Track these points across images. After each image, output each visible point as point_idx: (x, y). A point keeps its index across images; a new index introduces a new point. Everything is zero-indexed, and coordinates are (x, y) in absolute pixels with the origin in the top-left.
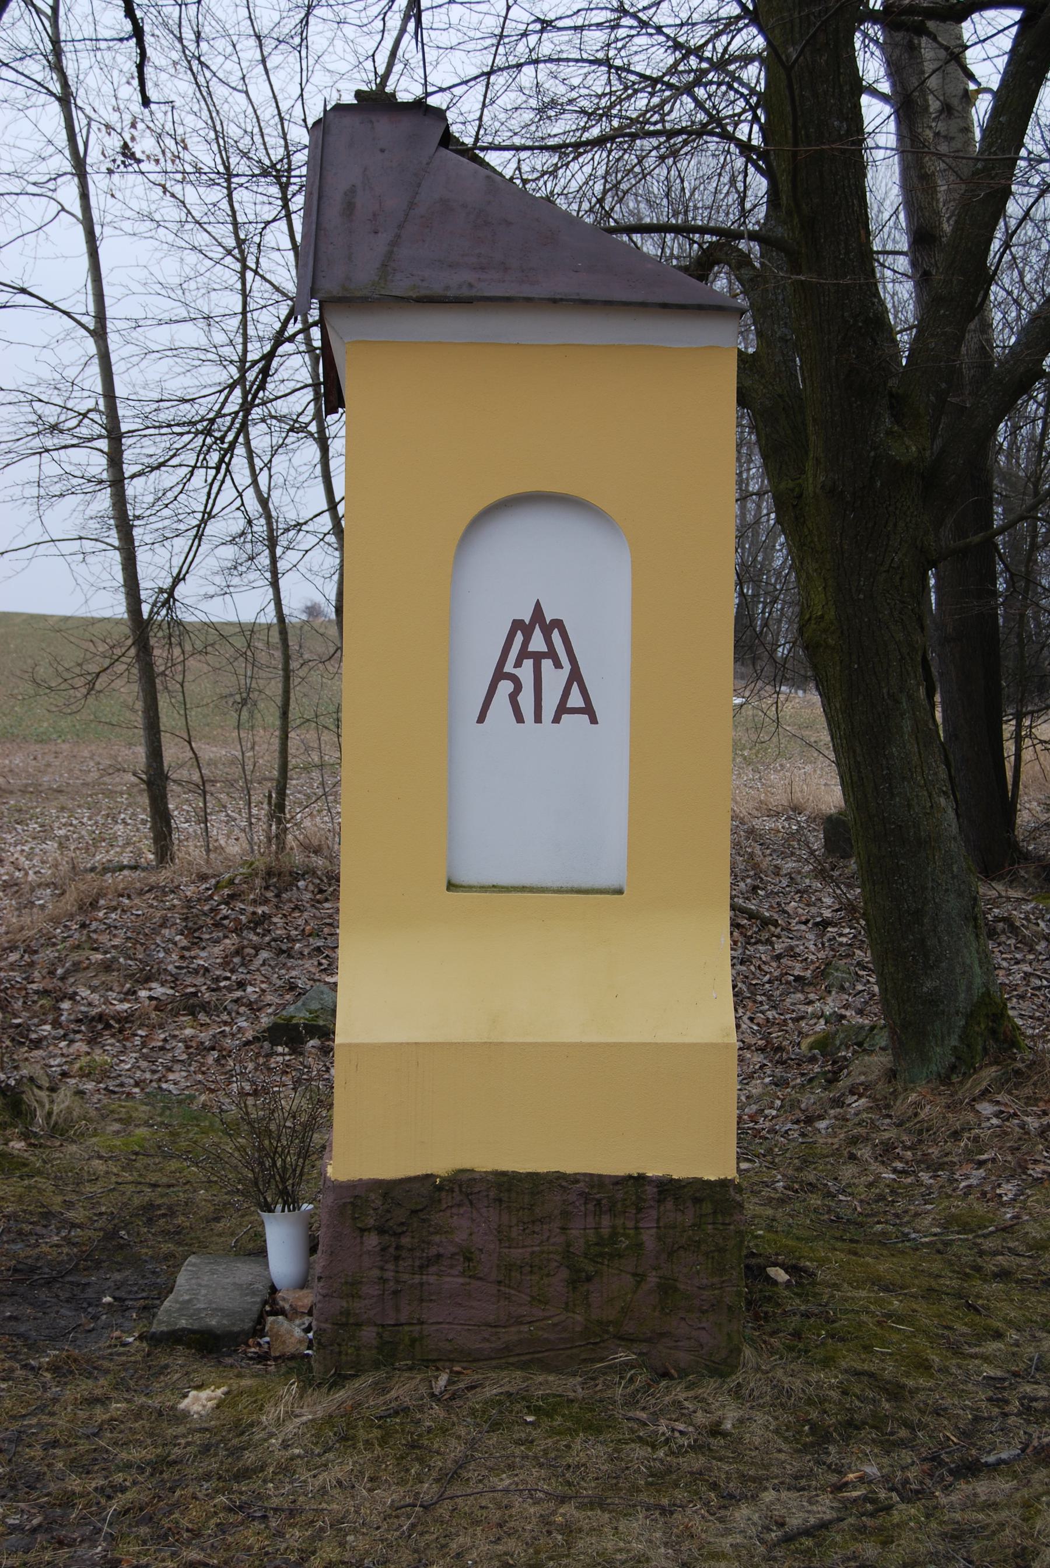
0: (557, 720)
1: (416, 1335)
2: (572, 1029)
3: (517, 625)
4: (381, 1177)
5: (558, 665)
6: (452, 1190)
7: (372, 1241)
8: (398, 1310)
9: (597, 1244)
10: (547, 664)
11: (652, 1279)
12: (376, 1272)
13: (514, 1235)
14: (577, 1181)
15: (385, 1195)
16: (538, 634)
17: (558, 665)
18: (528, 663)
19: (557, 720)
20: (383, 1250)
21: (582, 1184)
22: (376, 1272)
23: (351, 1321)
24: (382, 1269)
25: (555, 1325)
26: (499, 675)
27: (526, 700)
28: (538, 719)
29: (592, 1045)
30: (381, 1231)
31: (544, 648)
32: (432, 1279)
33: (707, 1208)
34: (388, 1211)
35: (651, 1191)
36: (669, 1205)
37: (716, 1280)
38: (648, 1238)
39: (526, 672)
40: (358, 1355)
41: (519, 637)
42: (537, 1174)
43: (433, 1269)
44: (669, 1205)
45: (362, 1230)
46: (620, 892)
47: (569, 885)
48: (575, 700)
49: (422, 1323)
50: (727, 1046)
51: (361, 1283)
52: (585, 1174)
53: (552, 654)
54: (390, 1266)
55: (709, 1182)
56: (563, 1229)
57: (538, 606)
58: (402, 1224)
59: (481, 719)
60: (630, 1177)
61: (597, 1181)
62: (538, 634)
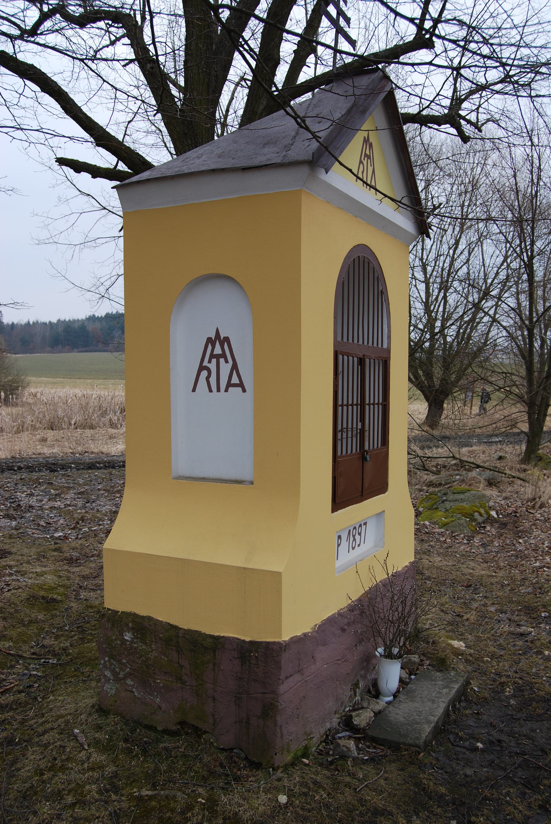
3: (209, 340)
16: (218, 345)
19: (226, 390)
26: (201, 368)
28: (218, 390)
48: (235, 380)
57: (217, 331)
59: (62, 162)
62: (218, 345)
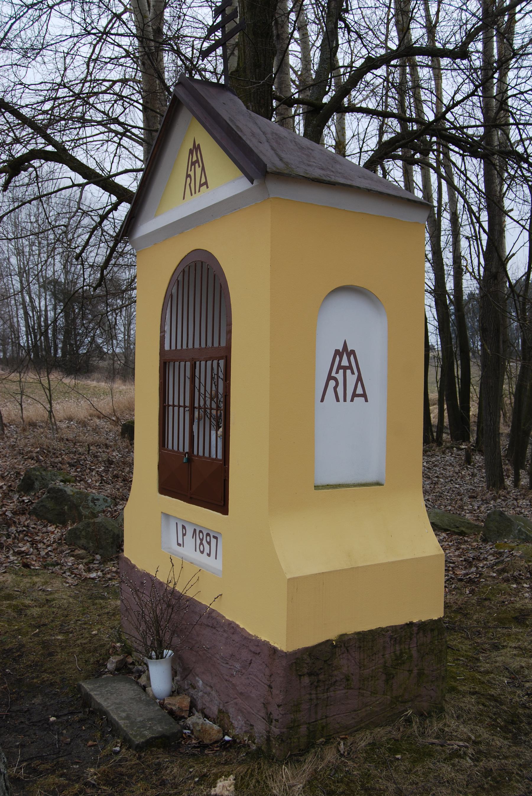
0: (352, 400)
1: (324, 724)
2: (382, 557)
3: (337, 352)
4: (307, 646)
5: (353, 373)
6: (341, 647)
7: (306, 680)
8: (316, 713)
9: (396, 660)
10: (348, 372)
11: (415, 671)
12: (308, 696)
13: (365, 663)
14: (388, 631)
15: (310, 655)
16: (345, 357)
17: (353, 373)
18: (341, 371)
19: (352, 400)
20: (311, 684)
21: (390, 632)
22: (308, 696)
23: (296, 724)
24: (310, 694)
25: (380, 703)
26: (330, 378)
27: (340, 390)
28: (345, 400)
29: (393, 563)
30: (310, 674)
31: (347, 364)
32: (332, 694)
33: (436, 633)
34: (313, 663)
35: (415, 629)
36: (421, 634)
37: (439, 666)
38: (414, 652)
39: (340, 377)
40: (299, 742)
41: (338, 359)
42: (372, 630)
43: (332, 689)
44: (421, 634)
45: (300, 676)
46: (378, 484)
47: (353, 482)
48: (359, 391)
49: (326, 717)
50: (441, 555)
51: (301, 704)
52: (390, 627)
53: (350, 367)
54: (314, 692)
55: (435, 620)
56: (383, 655)
58: (321, 669)
59: (322, 400)
60: (407, 624)
61: (394, 629)
62: (345, 357)
